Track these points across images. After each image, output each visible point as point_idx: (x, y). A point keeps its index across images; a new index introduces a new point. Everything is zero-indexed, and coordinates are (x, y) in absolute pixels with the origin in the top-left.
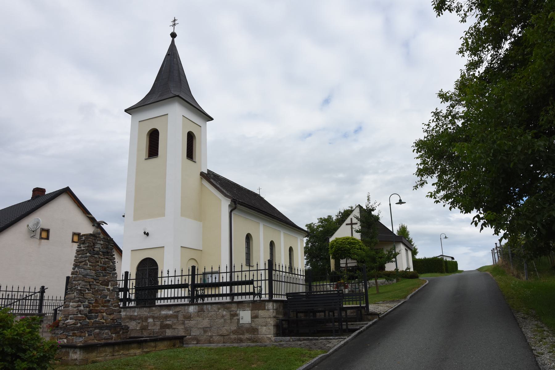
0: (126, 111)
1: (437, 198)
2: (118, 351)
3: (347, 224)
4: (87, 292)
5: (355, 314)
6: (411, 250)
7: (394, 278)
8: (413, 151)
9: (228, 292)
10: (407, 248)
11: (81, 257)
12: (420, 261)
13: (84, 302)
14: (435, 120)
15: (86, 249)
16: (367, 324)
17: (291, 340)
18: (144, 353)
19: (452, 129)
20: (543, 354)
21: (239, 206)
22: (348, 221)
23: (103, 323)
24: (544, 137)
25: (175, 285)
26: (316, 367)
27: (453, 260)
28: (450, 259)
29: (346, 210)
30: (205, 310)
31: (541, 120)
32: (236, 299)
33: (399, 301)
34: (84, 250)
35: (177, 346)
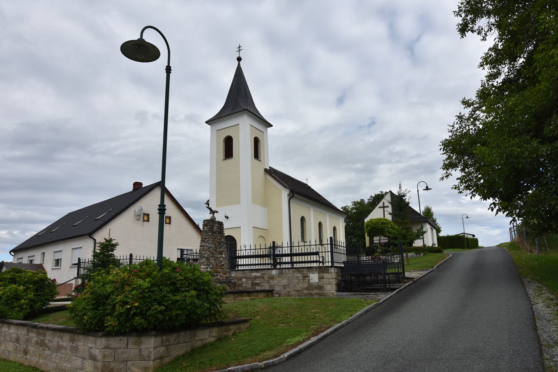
0: (206, 122)
1: (460, 190)
2: (237, 297)
3: (380, 207)
4: (211, 258)
5: (394, 278)
6: (435, 228)
7: (422, 252)
8: (440, 150)
9: (289, 261)
10: (432, 227)
11: (206, 235)
12: (444, 238)
13: (210, 265)
14: (459, 122)
15: (209, 230)
16: (404, 285)
17: (349, 295)
18: (251, 300)
19: (473, 129)
20: (538, 304)
21: (295, 195)
22: (381, 204)
23: (221, 280)
24: (547, 143)
25: (256, 255)
26: (373, 310)
27: (474, 237)
28: (471, 237)
29: (376, 194)
30: (284, 273)
31: (545, 130)
32: (295, 266)
33: (427, 270)
34: (207, 230)
35: (270, 296)
